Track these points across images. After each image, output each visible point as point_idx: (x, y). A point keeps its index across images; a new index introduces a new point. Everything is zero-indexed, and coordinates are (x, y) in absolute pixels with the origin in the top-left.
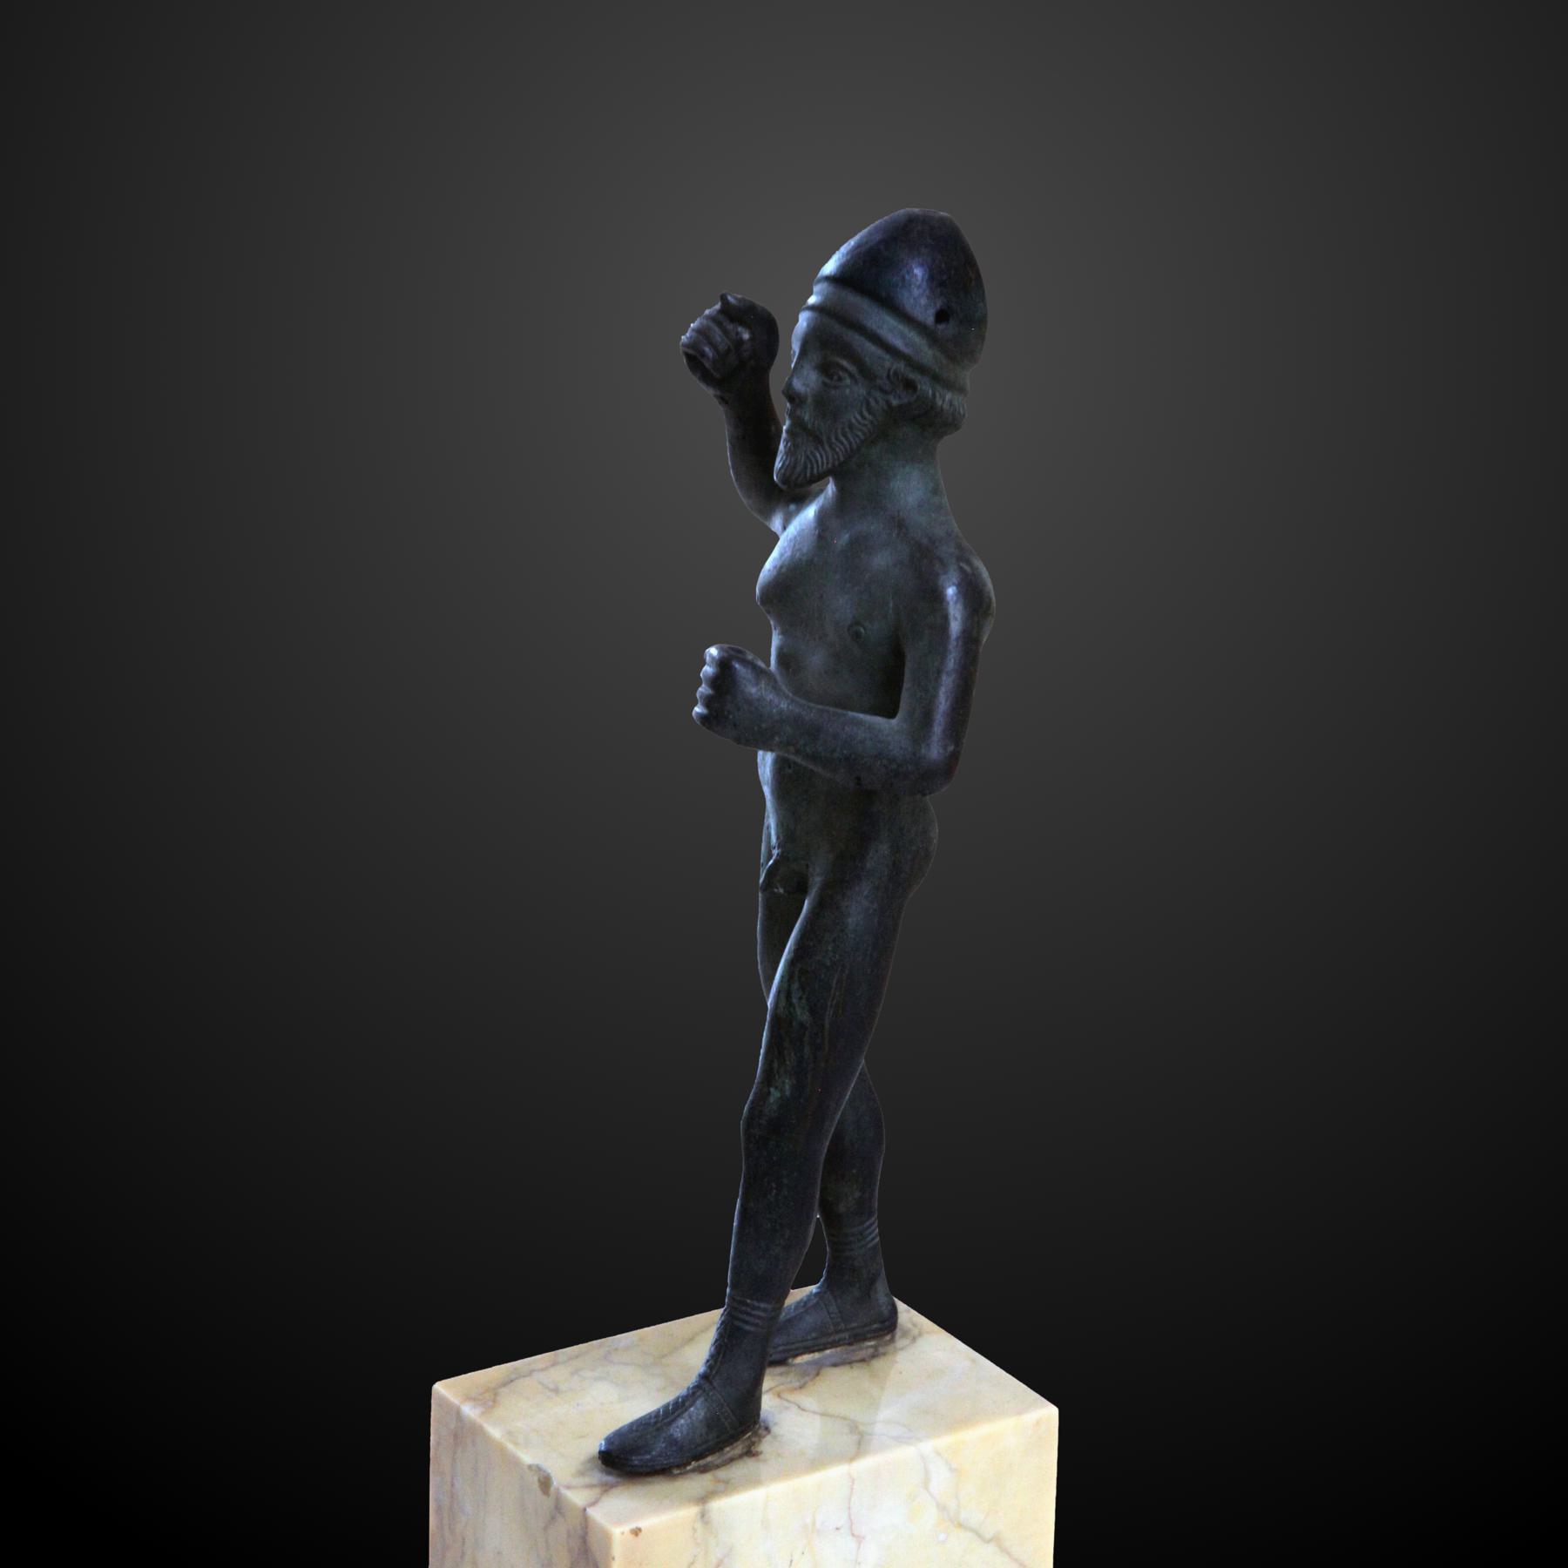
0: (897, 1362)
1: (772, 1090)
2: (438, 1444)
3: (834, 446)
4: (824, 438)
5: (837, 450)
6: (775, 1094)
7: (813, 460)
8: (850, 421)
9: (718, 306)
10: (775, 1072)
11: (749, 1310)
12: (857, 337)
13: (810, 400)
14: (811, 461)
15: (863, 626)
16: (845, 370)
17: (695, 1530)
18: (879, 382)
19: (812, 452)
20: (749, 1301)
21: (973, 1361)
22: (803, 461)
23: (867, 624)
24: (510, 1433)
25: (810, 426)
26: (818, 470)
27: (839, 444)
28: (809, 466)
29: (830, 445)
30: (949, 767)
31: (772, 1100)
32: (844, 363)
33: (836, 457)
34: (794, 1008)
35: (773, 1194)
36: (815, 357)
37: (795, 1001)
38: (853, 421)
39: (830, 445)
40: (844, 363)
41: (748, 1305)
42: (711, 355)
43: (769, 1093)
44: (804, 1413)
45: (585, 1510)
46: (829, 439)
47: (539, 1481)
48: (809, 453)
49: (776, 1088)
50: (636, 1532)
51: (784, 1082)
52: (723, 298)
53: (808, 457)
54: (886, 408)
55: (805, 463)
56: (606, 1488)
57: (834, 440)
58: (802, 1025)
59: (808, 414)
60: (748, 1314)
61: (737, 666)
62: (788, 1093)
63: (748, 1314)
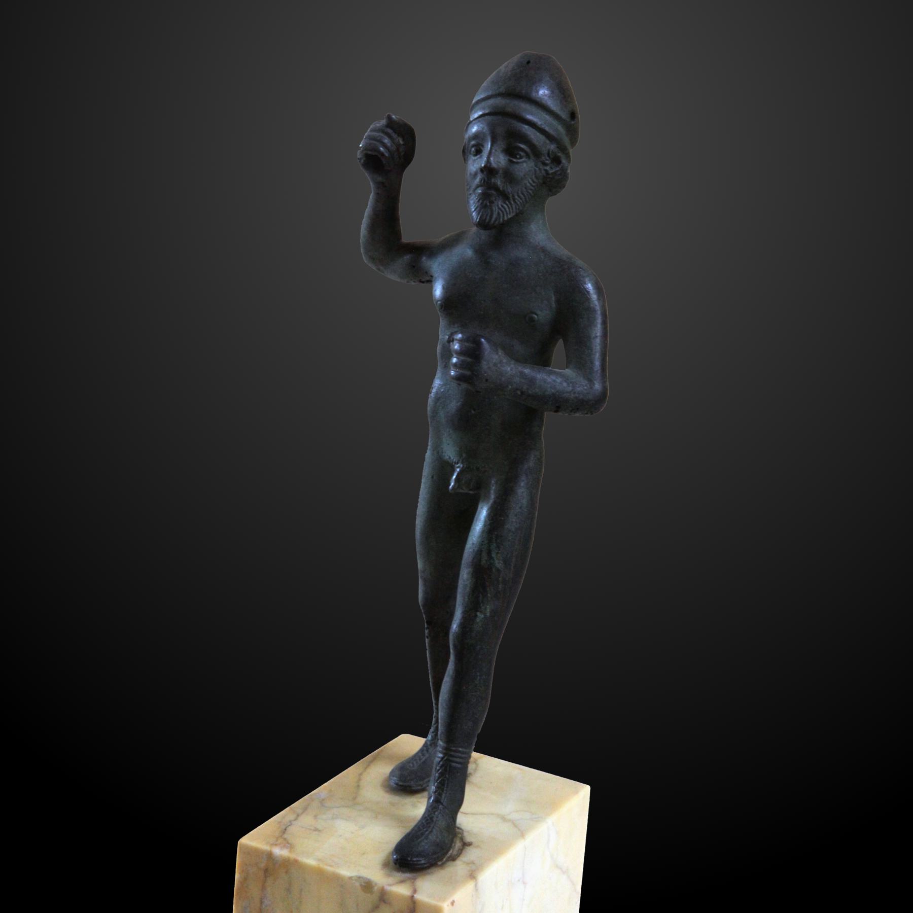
0: (470, 774)
1: (478, 614)
2: (245, 879)
3: (516, 201)
4: (511, 196)
5: (518, 203)
6: (480, 616)
7: (503, 210)
8: (525, 184)
9: (383, 122)
10: (481, 602)
11: (460, 755)
12: (526, 127)
13: (501, 172)
14: (502, 211)
15: (536, 314)
16: (522, 150)
17: (473, 896)
18: (543, 158)
19: (502, 206)
20: (460, 749)
21: (519, 769)
22: (497, 211)
23: (539, 312)
24: (319, 860)
25: (501, 189)
26: (503, 219)
27: (519, 199)
28: (502, 215)
29: (514, 200)
30: (604, 394)
31: (478, 620)
32: (522, 146)
33: (517, 207)
34: (494, 560)
35: (478, 679)
36: (501, 144)
37: (494, 555)
38: (528, 184)
39: (514, 200)
40: (522, 146)
41: (459, 752)
42: (387, 155)
43: (476, 616)
44: (467, 815)
45: (413, 897)
46: (513, 196)
47: (361, 885)
48: (500, 206)
49: (481, 612)
50: (453, 903)
51: (486, 608)
52: (389, 118)
53: (499, 208)
54: (545, 175)
55: (499, 213)
56: (415, 879)
57: (516, 197)
58: (498, 570)
59: (499, 181)
60: (460, 758)
61: (483, 340)
62: (488, 614)
63: (460, 758)
